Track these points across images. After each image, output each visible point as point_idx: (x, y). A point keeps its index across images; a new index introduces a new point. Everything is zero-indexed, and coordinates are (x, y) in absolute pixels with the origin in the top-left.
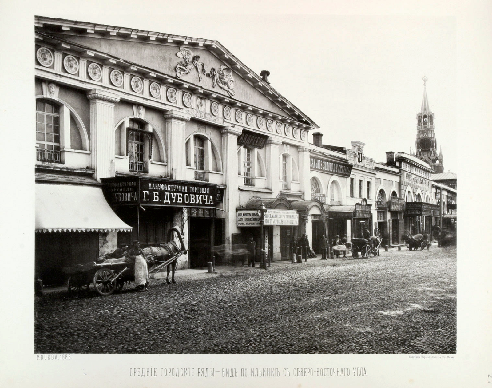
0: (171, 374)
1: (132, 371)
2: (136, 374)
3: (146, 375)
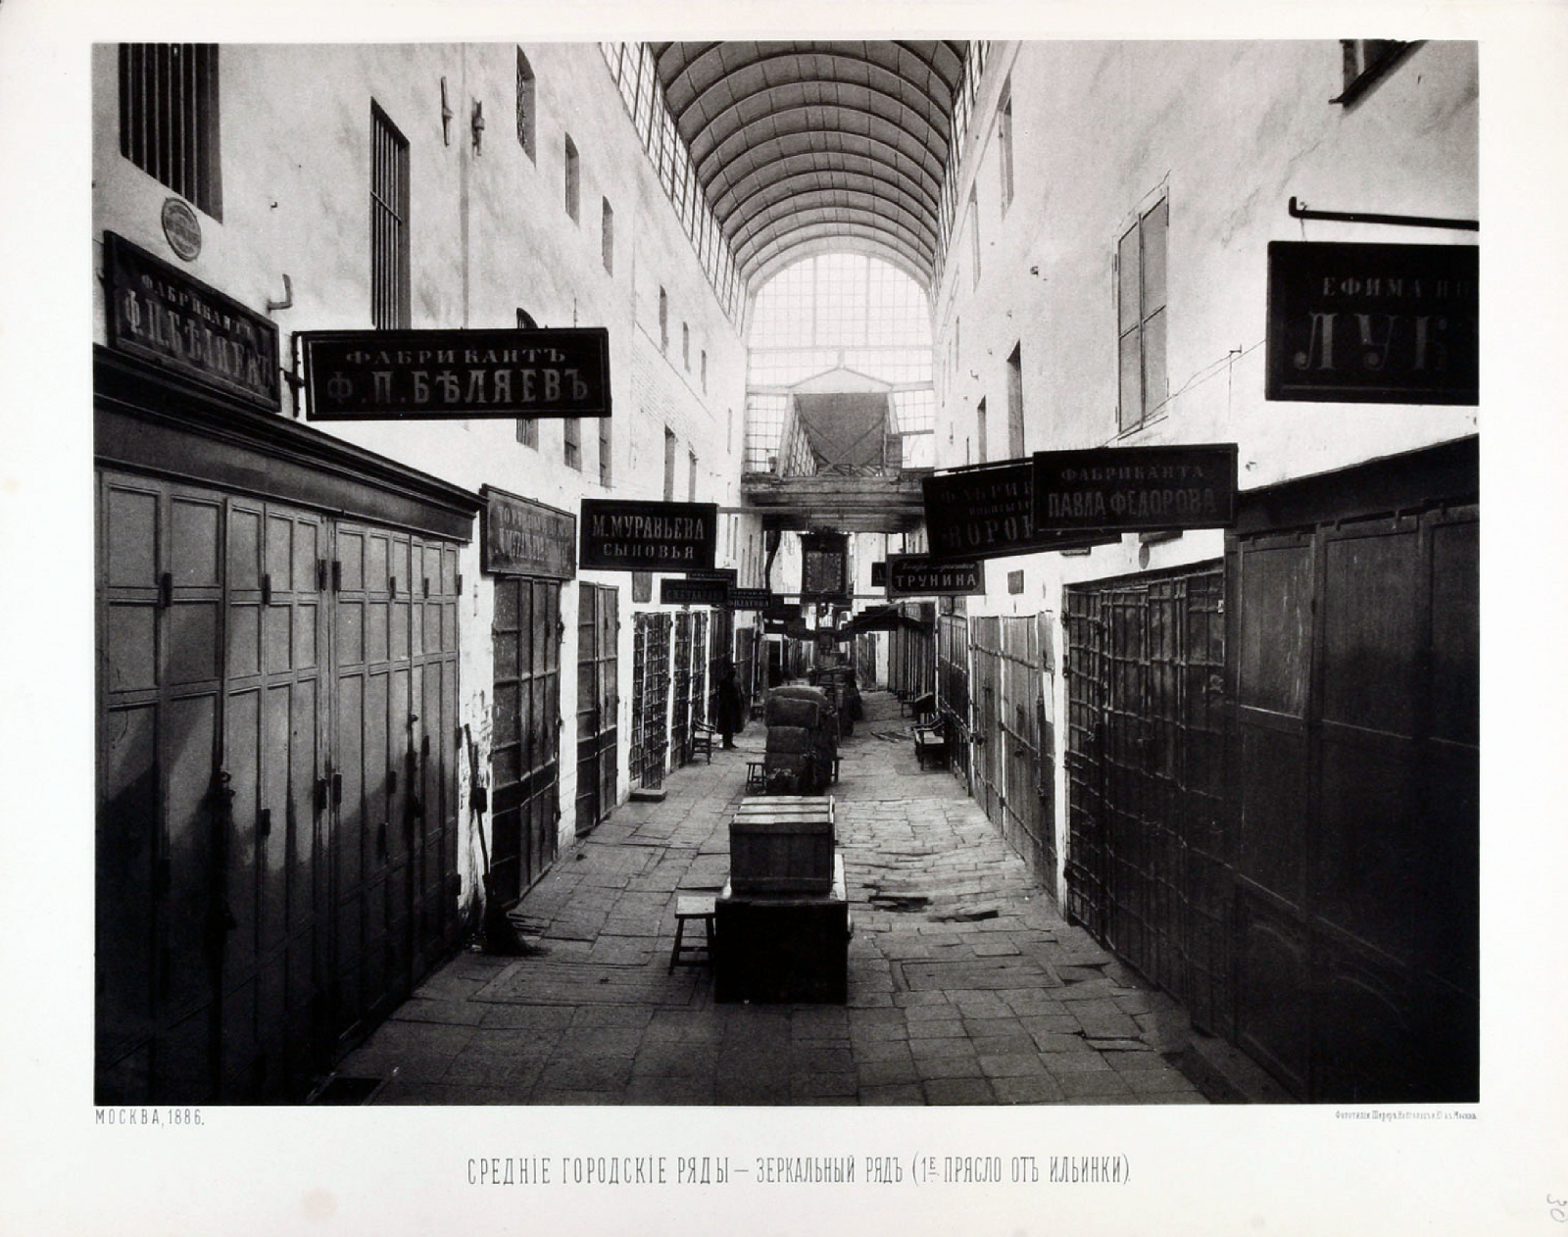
1: (476, 1170)
2: (488, 1177)
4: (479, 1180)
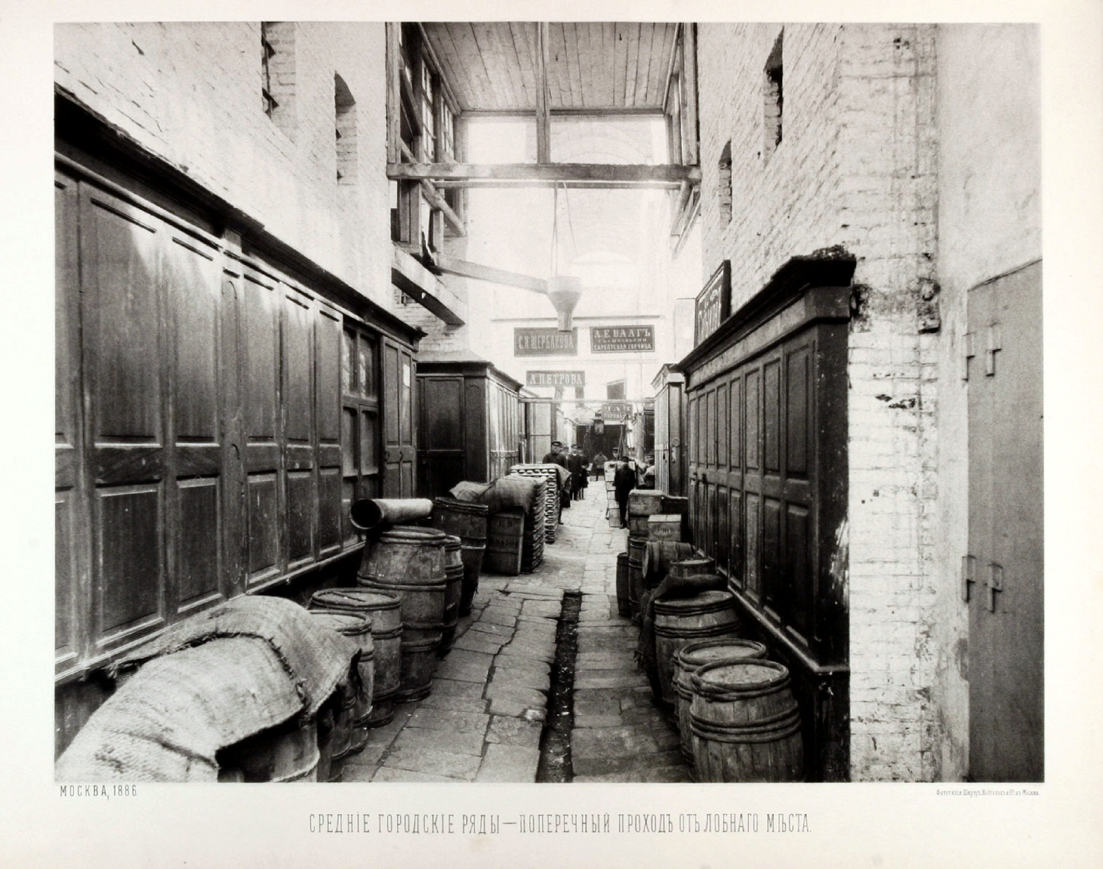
0: (401, 827)
1: (315, 822)
2: (324, 828)
3: (345, 828)
4: (317, 829)
